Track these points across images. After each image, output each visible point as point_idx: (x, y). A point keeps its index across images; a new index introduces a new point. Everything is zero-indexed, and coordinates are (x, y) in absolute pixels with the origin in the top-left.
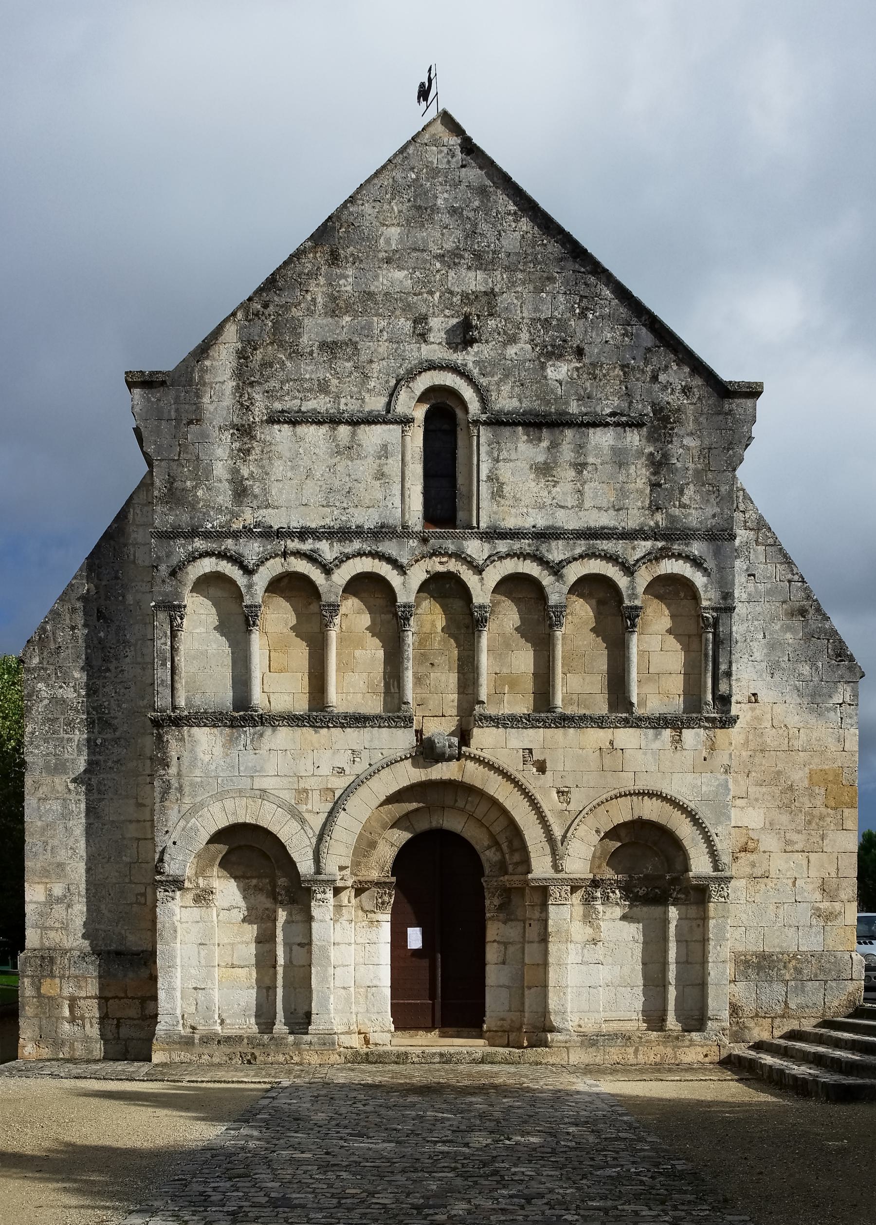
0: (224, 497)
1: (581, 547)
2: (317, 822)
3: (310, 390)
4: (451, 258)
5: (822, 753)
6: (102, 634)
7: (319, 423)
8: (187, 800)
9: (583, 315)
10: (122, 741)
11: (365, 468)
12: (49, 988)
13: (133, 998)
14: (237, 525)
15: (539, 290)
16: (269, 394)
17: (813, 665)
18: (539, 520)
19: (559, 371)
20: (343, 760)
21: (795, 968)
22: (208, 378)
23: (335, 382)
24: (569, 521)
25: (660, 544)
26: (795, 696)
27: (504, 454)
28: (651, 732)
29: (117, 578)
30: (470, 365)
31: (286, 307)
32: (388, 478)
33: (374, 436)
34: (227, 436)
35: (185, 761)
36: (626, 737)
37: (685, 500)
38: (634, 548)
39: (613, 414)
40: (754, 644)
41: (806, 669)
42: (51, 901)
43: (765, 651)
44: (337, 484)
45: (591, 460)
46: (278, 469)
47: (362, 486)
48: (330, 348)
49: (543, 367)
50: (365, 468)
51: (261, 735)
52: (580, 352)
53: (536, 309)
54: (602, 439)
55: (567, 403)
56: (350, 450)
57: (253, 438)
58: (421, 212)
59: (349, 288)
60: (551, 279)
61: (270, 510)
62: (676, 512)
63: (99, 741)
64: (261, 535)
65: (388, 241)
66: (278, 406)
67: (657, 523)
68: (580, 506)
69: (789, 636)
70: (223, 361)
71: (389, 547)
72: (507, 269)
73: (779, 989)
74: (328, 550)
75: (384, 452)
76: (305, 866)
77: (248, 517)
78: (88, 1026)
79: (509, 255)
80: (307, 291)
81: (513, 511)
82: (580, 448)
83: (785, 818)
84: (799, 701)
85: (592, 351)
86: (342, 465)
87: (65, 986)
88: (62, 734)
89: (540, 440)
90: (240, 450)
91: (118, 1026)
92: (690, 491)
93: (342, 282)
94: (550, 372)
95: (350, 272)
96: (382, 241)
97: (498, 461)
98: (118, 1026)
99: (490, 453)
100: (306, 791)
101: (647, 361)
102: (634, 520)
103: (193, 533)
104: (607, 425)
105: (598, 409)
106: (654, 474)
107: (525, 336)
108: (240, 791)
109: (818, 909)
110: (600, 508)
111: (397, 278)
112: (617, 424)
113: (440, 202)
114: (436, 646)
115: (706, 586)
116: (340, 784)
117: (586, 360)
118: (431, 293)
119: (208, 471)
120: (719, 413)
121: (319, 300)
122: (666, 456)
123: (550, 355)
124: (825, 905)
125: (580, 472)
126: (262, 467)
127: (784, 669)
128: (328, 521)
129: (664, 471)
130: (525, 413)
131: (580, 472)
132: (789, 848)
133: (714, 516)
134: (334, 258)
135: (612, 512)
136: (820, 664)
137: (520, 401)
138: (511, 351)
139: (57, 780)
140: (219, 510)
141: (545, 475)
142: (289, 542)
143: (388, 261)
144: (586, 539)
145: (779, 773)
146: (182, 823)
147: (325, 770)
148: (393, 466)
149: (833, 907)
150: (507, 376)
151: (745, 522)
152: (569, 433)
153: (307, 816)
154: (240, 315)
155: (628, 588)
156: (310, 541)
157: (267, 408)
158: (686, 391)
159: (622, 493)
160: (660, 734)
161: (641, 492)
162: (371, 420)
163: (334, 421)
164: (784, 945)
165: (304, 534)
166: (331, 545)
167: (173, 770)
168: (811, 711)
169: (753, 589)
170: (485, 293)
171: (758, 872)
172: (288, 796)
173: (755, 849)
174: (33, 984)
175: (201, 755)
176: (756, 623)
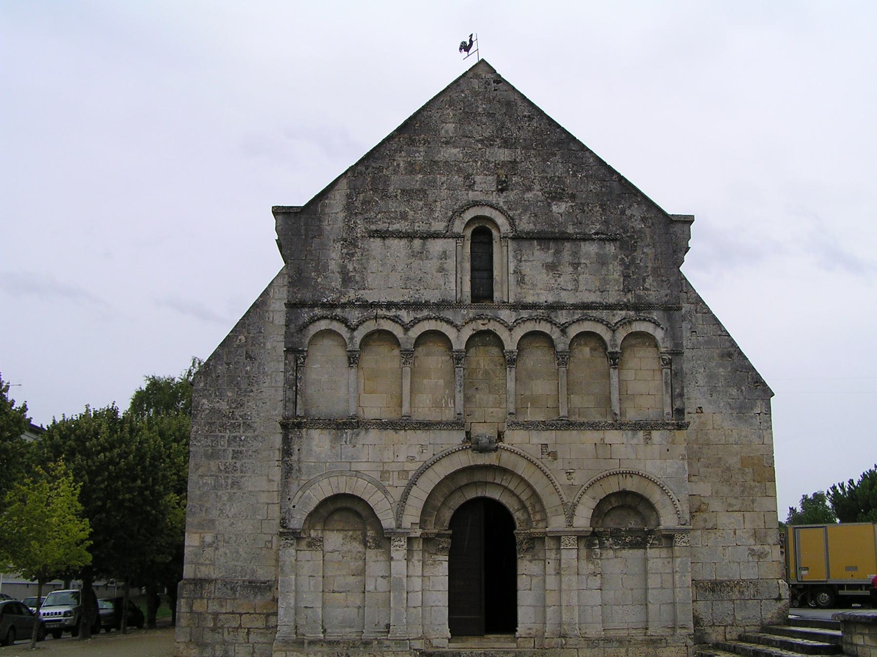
0: (336, 282)
2: (397, 494)
3: (395, 218)
4: (488, 142)
6: (248, 368)
7: (401, 238)
9: (575, 175)
10: (260, 438)
11: (432, 265)
12: (198, 606)
13: (260, 614)
14: (343, 300)
15: (544, 161)
16: (368, 220)
17: (739, 389)
19: (559, 208)
20: (414, 451)
22: (327, 210)
24: (568, 298)
26: (728, 408)
28: (630, 433)
29: (260, 332)
30: (501, 204)
31: (380, 169)
32: (444, 271)
33: (436, 246)
34: (338, 245)
35: (304, 452)
36: (613, 436)
37: (647, 285)
38: (614, 315)
39: (596, 233)
40: (699, 376)
41: (734, 392)
42: (203, 545)
44: (412, 275)
45: (583, 261)
46: (373, 265)
47: (429, 276)
48: (408, 194)
50: (432, 265)
51: (358, 435)
52: (573, 197)
54: (590, 249)
56: (421, 255)
57: (357, 246)
58: (468, 115)
59: (421, 158)
60: (555, 155)
61: (367, 291)
62: (642, 293)
63: (243, 438)
64: (360, 306)
65: (447, 132)
66: (373, 227)
67: (628, 300)
68: (576, 290)
69: (721, 370)
70: (338, 200)
71: (448, 314)
72: (523, 148)
74: (406, 316)
75: (444, 255)
76: (388, 522)
77: (352, 295)
78: (226, 633)
80: (394, 160)
81: (531, 292)
82: (575, 254)
83: (725, 489)
84: (730, 411)
86: (416, 263)
87: (210, 604)
88: (218, 433)
90: (347, 254)
91: (248, 634)
92: (649, 281)
93: (417, 155)
94: (554, 208)
98: (248, 634)
99: (515, 257)
100: (388, 472)
101: (619, 203)
102: (612, 298)
103: (313, 306)
104: (593, 240)
105: (587, 231)
107: (537, 187)
108: (342, 471)
109: (753, 550)
110: (590, 291)
111: (452, 153)
112: (600, 239)
115: (663, 339)
118: (476, 162)
119: (326, 267)
122: (633, 259)
123: (553, 199)
124: (757, 548)
126: (362, 264)
128: (406, 298)
133: (666, 295)
134: (412, 142)
135: (598, 293)
138: (529, 195)
139: (212, 463)
140: (333, 291)
141: (552, 270)
142: (379, 310)
143: (447, 143)
145: (720, 459)
146: (300, 493)
147: (402, 458)
148: (450, 264)
151: (688, 299)
152: (568, 245)
153: (388, 489)
154: (349, 174)
156: (394, 310)
157: (366, 228)
158: (644, 220)
159: (605, 281)
160: (636, 434)
161: (617, 281)
162: (436, 236)
163: (410, 236)
165: (389, 305)
166: (408, 312)
167: (295, 458)
171: (710, 525)
172: (376, 476)
174: (187, 603)
175: (315, 448)
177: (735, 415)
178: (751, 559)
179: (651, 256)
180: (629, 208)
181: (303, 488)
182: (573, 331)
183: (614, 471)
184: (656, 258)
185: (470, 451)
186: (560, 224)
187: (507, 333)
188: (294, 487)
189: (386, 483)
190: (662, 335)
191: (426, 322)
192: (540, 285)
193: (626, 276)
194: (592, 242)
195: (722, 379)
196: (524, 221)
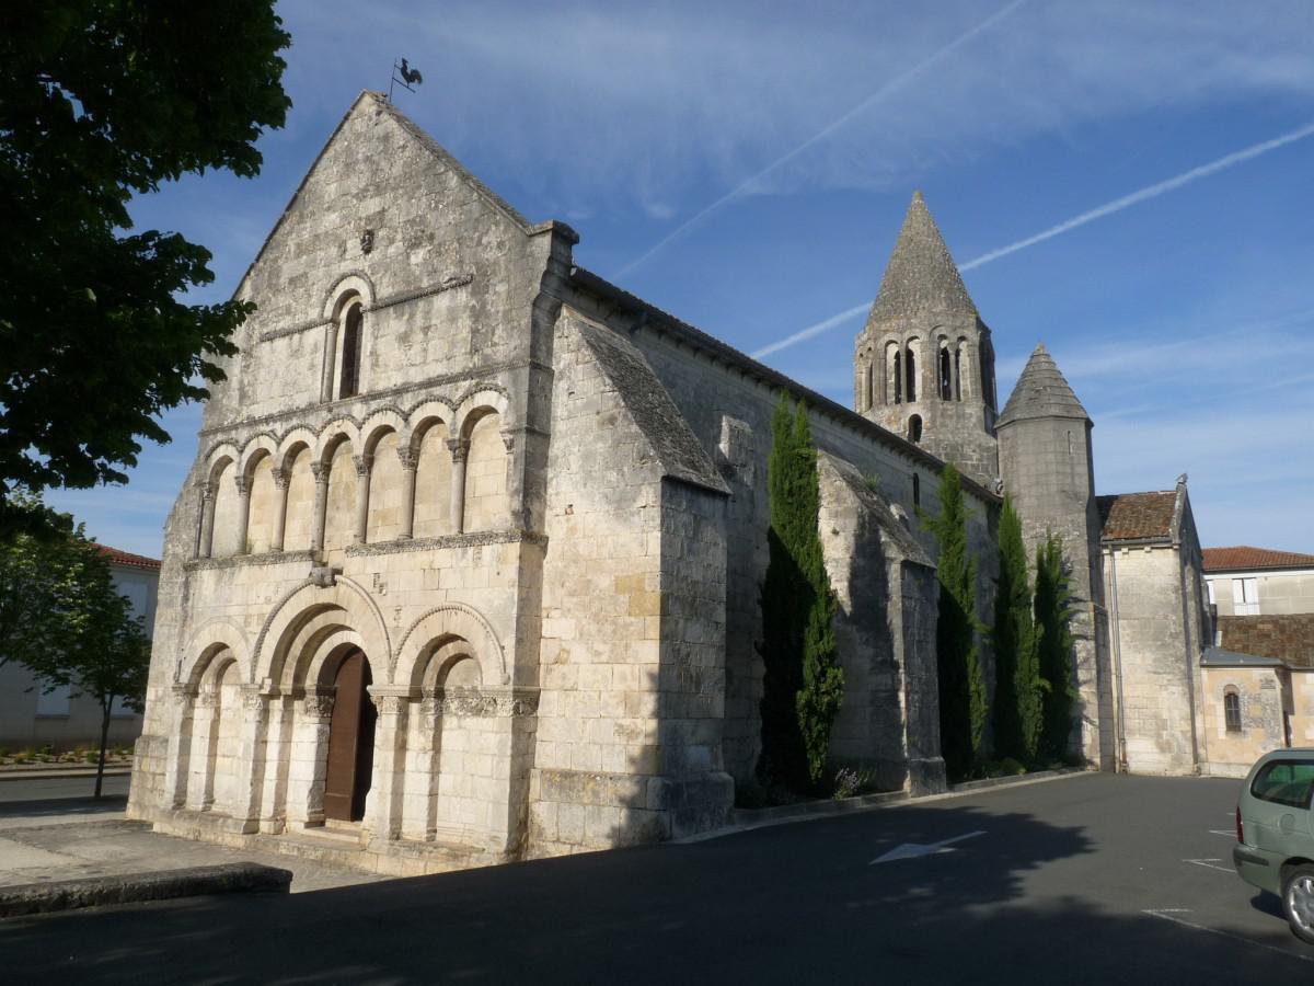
0: (235, 403)
1: (423, 394)
2: (254, 640)
3: (281, 315)
4: (361, 195)
5: (627, 559)
8: (194, 626)
16: (263, 324)
17: (620, 471)
18: (397, 380)
21: (593, 791)
23: (294, 304)
25: (474, 382)
27: (381, 333)
28: (459, 551)
37: (496, 339)
38: (457, 390)
40: (572, 458)
41: (613, 476)
43: (580, 463)
45: (433, 322)
46: (262, 374)
49: (408, 257)
50: (304, 363)
53: (408, 213)
54: (442, 302)
55: (421, 281)
56: (296, 353)
60: (419, 187)
61: (255, 406)
62: (488, 351)
67: (475, 364)
69: (600, 445)
73: (578, 811)
74: (279, 428)
79: (395, 179)
81: (383, 375)
85: (440, 234)
89: (403, 315)
92: (499, 331)
95: (308, 225)
96: (326, 197)
97: (376, 338)
103: (216, 431)
104: (444, 290)
106: (474, 323)
109: (621, 726)
110: (437, 361)
112: (453, 287)
113: (360, 156)
114: (342, 492)
116: (268, 609)
117: (436, 242)
118: (349, 223)
120: (523, 257)
121: (292, 250)
122: (483, 306)
124: (627, 722)
125: (426, 334)
127: (595, 478)
128: (283, 408)
129: (482, 318)
130: (396, 295)
131: (426, 334)
132: (596, 660)
133: (515, 348)
135: (445, 362)
136: (626, 469)
137: (393, 287)
138: (392, 250)
140: (232, 412)
143: (329, 209)
144: (426, 388)
149: (635, 724)
150: (386, 271)
155: (451, 425)
159: (453, 344)
163: (287, 333)
164: (589, 764)
167: (190, 603)
168: (617, 516)
169: (572, 406)
170: (379, 212)
173: (567, 659)
176: (574, 437)
177: (612, 512)
178: (617, 740)
179: (504, 296)
180: (487, 233)
181: (192, 638)
182: (417, 418)
183: (440, 606)
184: (509, 297)
185: (313, 586)
186: (416, 278)
187: (357, 431)
188: (187, 637)
189: (248, 629)
190: (505, 407)
191: (418, 410)
192: (392, 366)
193: (474, 332)
194: (443, 293)
195: (599, 458)
196: (384, 285)
